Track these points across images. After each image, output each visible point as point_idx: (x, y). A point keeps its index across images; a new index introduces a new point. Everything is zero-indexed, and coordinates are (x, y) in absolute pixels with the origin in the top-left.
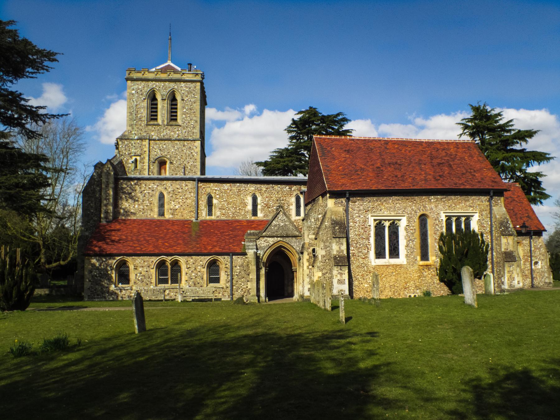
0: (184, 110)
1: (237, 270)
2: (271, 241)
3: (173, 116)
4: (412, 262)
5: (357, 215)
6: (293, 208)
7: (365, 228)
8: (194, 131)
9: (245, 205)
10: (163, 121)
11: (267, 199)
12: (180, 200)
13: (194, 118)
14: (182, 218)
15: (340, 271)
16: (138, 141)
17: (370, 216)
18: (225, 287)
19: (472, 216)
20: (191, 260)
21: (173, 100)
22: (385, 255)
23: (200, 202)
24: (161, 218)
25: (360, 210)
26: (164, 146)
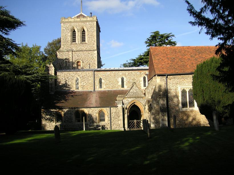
0: (89, 36)
2: (130, 100)
3: (83, 40)
5: (172, 86)
6: (142, 83)
8: (94, 46)
11: (129, 79)
12: (86, 81)
13: (94, 40)
15: (163, 114)
16: (67, 52)
18: (107, 123)
21: (74, 40)
22: (187, 106)
23: (95, 82)
26: (79, 54)
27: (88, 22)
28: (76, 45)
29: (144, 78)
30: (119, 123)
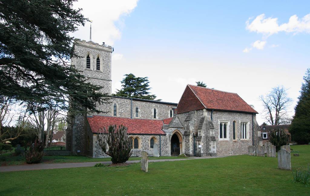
1: (162, 142)
3: (98, 68)
4: (231, 140)
7: (217, 125)
9: (152, 113)
10: (94, 69)
14: (125, 117)
17: (219, 120)
19: (247, 122)
20: (144, 137)
24: (115, 116)
25: (216, 118)
28: (91, 72)
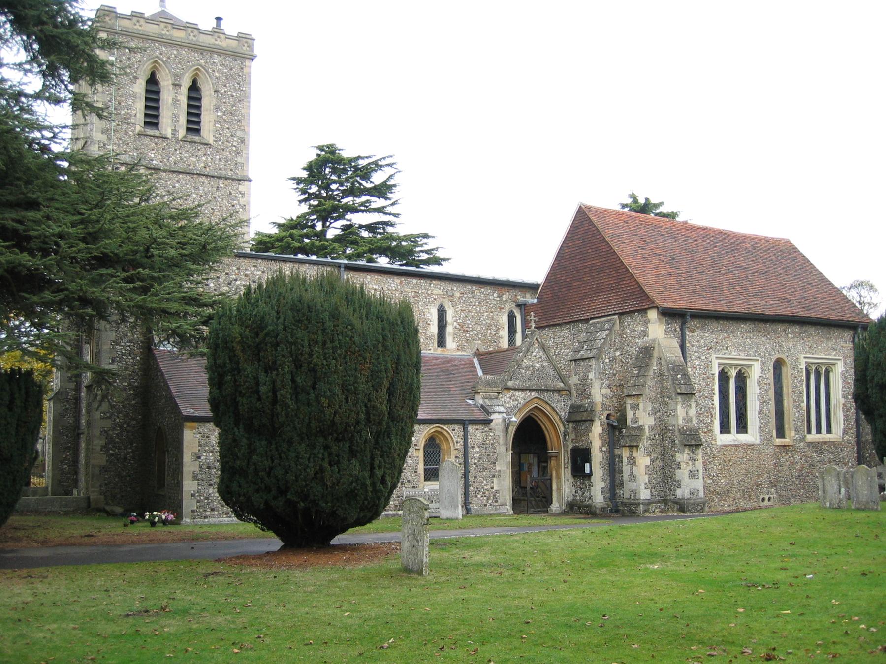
1: (475, 453)
3: (194, 126)
10: (175, 131)
11: (463, 315)
27: (219, 54)
29: (511, 318)
30: (496, 488)
